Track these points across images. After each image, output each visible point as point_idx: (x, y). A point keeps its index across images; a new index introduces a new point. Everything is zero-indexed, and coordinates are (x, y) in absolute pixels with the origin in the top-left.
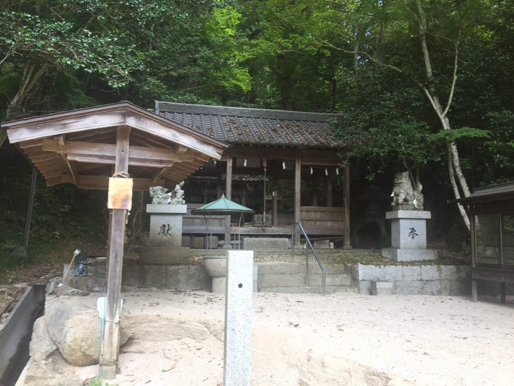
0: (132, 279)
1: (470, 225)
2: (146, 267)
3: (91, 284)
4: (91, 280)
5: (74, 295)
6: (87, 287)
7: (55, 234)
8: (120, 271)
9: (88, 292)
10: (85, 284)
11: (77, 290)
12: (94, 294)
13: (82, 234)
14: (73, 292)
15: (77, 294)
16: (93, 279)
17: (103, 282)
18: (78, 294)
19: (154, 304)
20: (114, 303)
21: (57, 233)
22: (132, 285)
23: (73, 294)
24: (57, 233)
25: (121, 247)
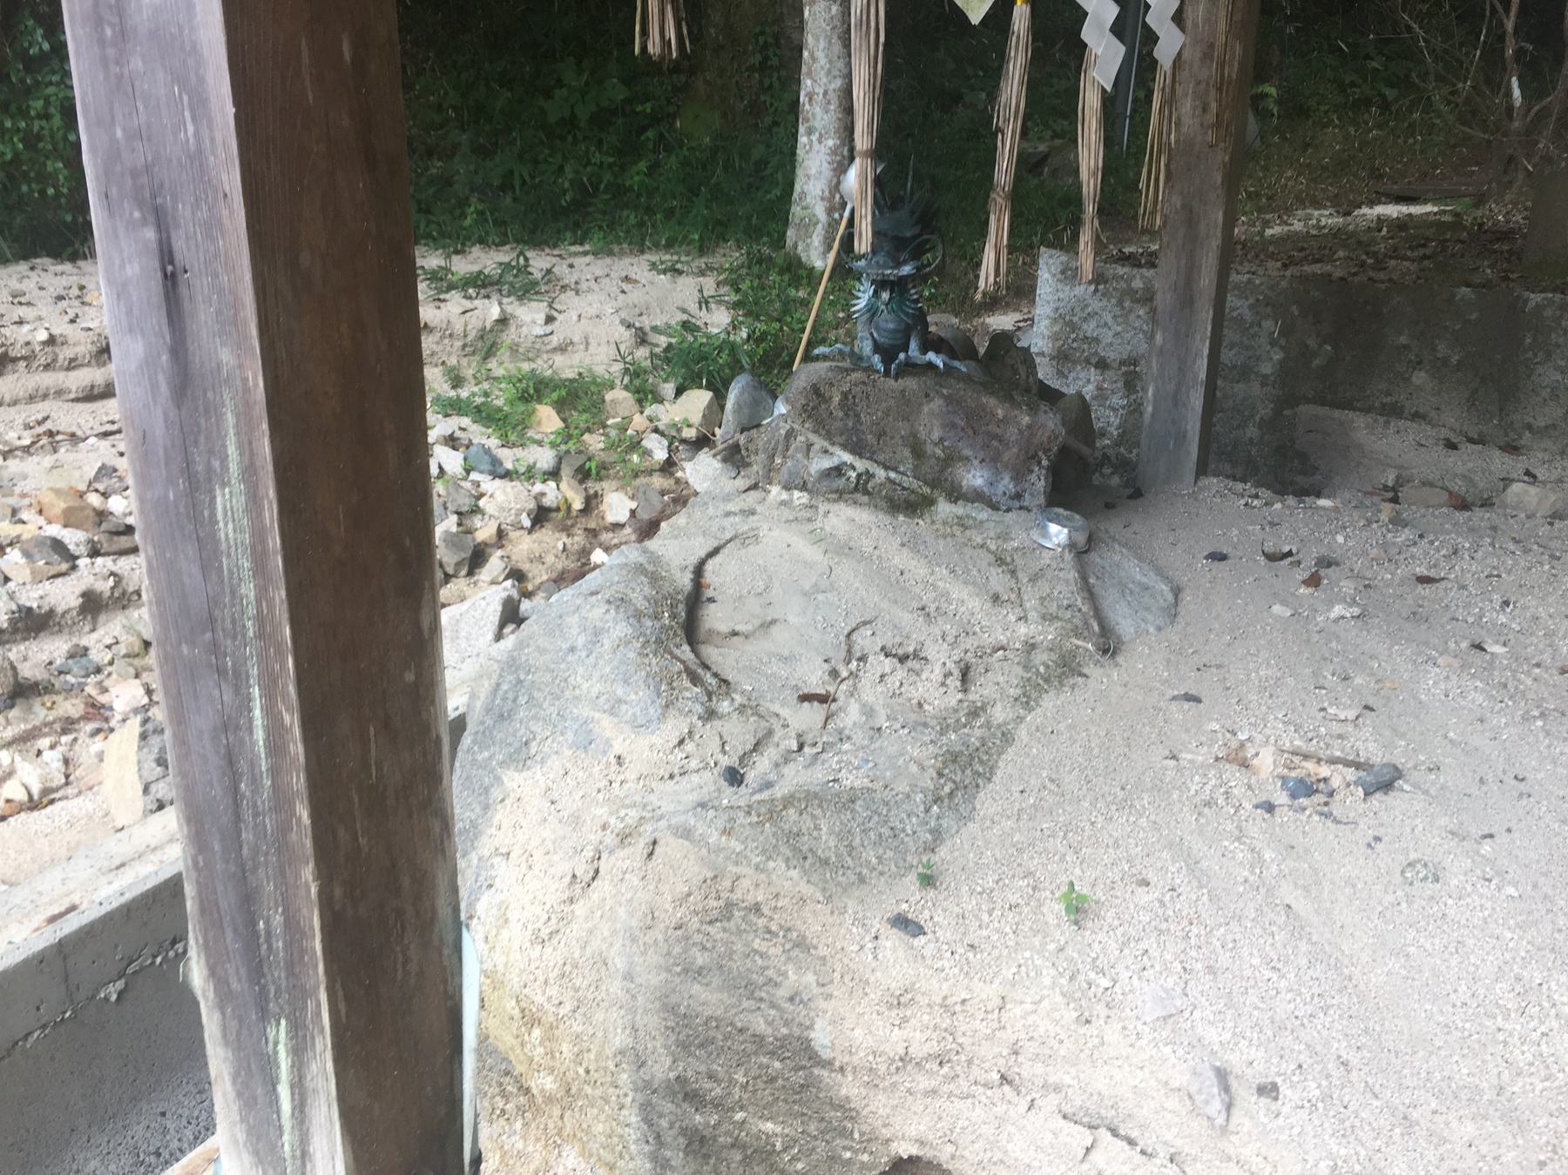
0: (1419, 377)
1: (1434, 205)
2: (1535, 298)
3: (936, 435)
4: (937, 404)
5: (841, 495)
6: (918, 452)
7: (1265, 96)
8: (259, 535)
9: (927, 490)
10: (903, 428)
11: (861, 465)
12: (959, 509)
13: (1390, 93)
14: (838, 471)
15: (861, 489)
16: (949, 399)
17: (1012, 433)
18: (866, 492)
19: (1339, 777)
20: (264, 1016)
21: (1273, 91)
22: (1416, 416)
23: (837, 486)
24: (1273, 91)
25: (200, 105)
